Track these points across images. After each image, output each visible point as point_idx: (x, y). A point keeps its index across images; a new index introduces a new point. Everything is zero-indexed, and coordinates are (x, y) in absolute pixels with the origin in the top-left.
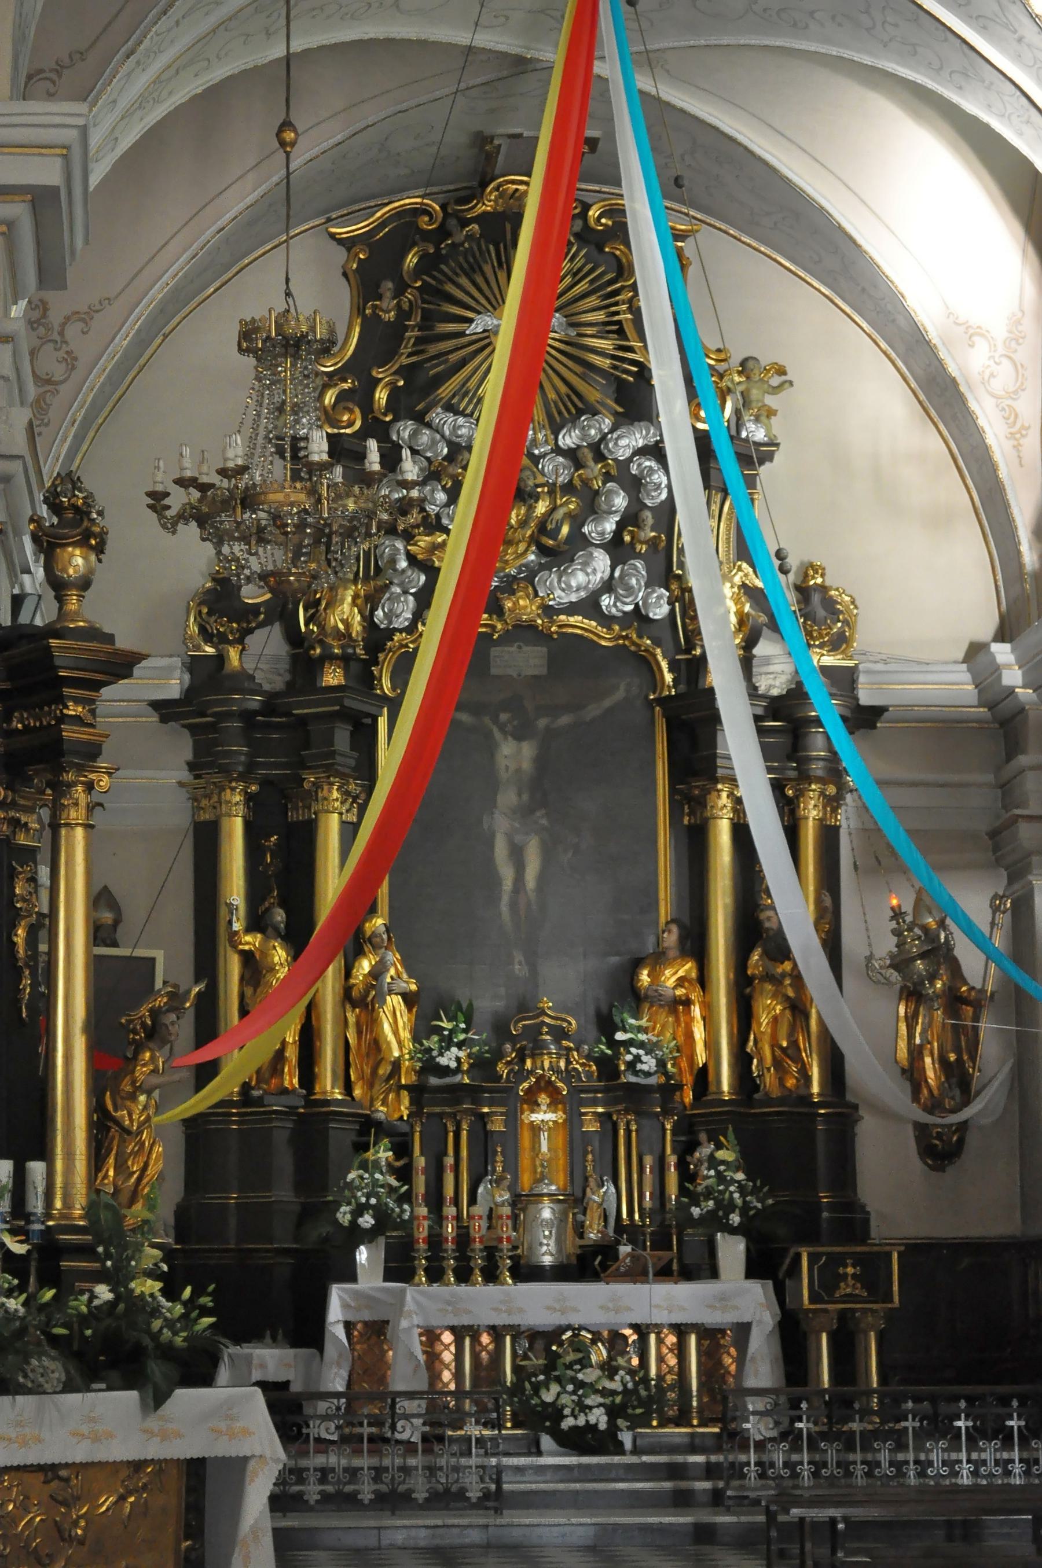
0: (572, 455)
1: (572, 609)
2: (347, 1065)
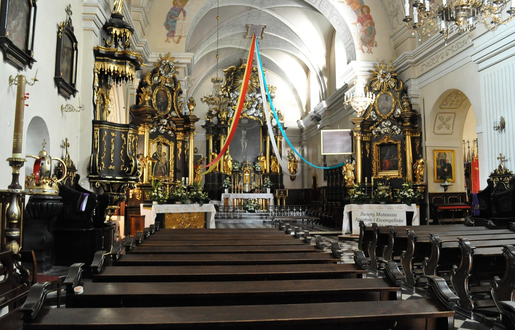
0: (251, 97)
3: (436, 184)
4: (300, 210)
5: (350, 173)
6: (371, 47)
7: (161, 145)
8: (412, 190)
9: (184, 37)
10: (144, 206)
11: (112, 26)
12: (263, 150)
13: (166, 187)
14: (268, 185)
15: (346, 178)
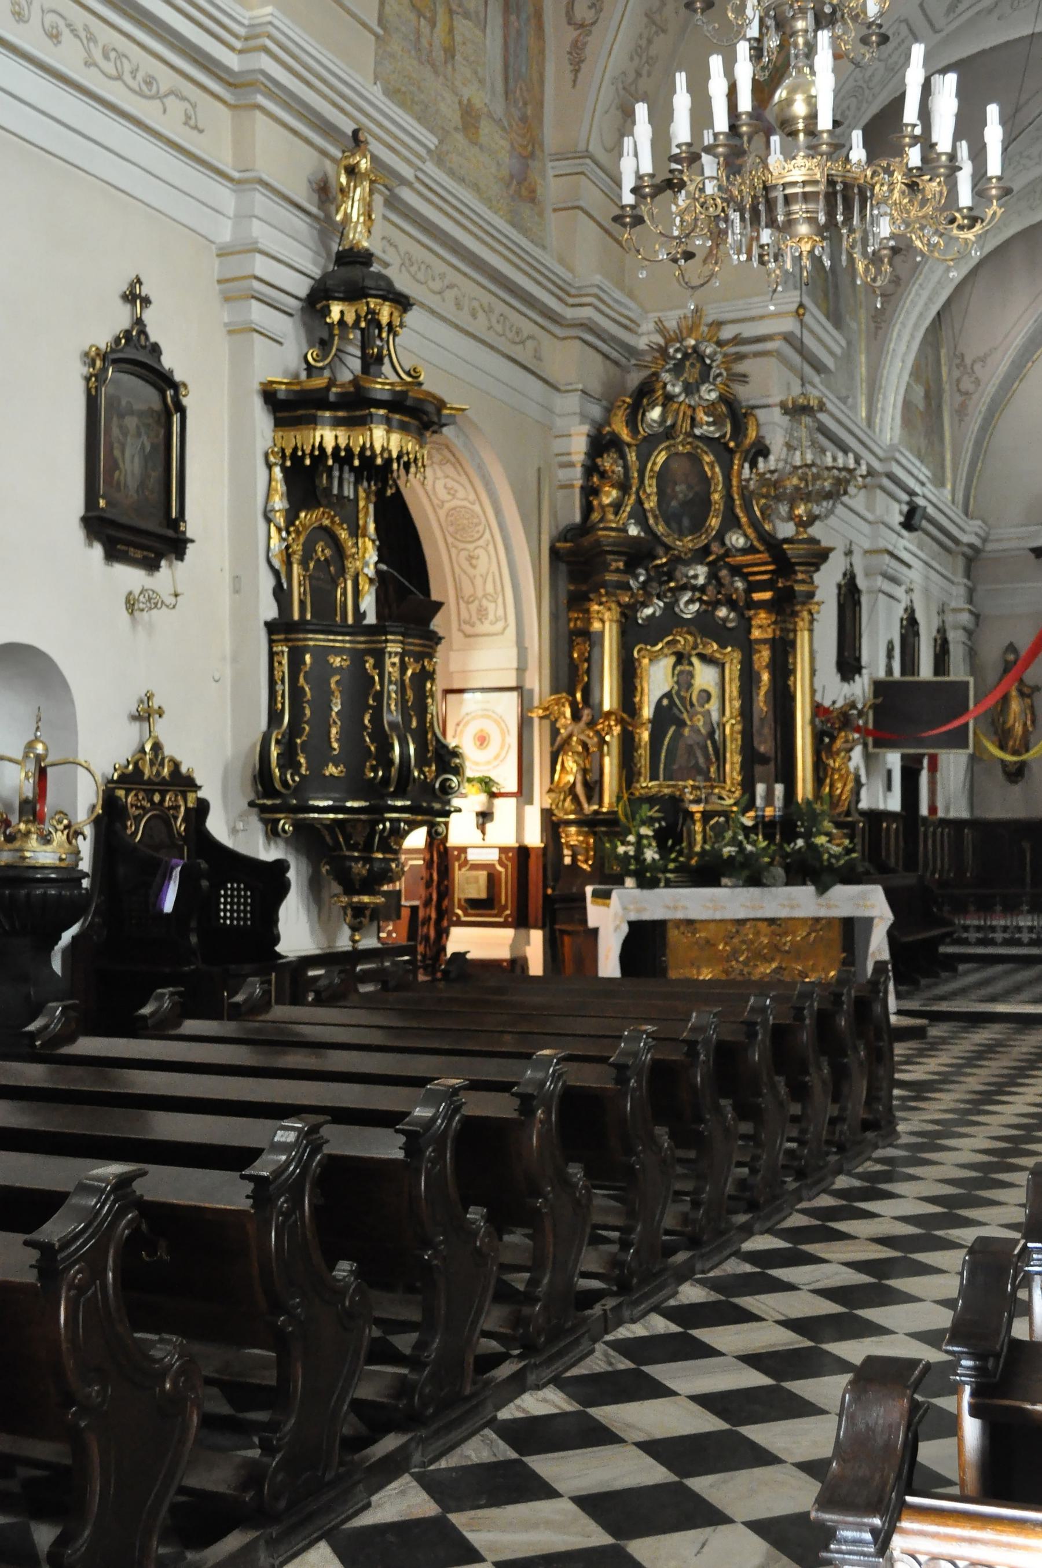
7: (691, 664)
10: (596, 894)
11: (328, 300)
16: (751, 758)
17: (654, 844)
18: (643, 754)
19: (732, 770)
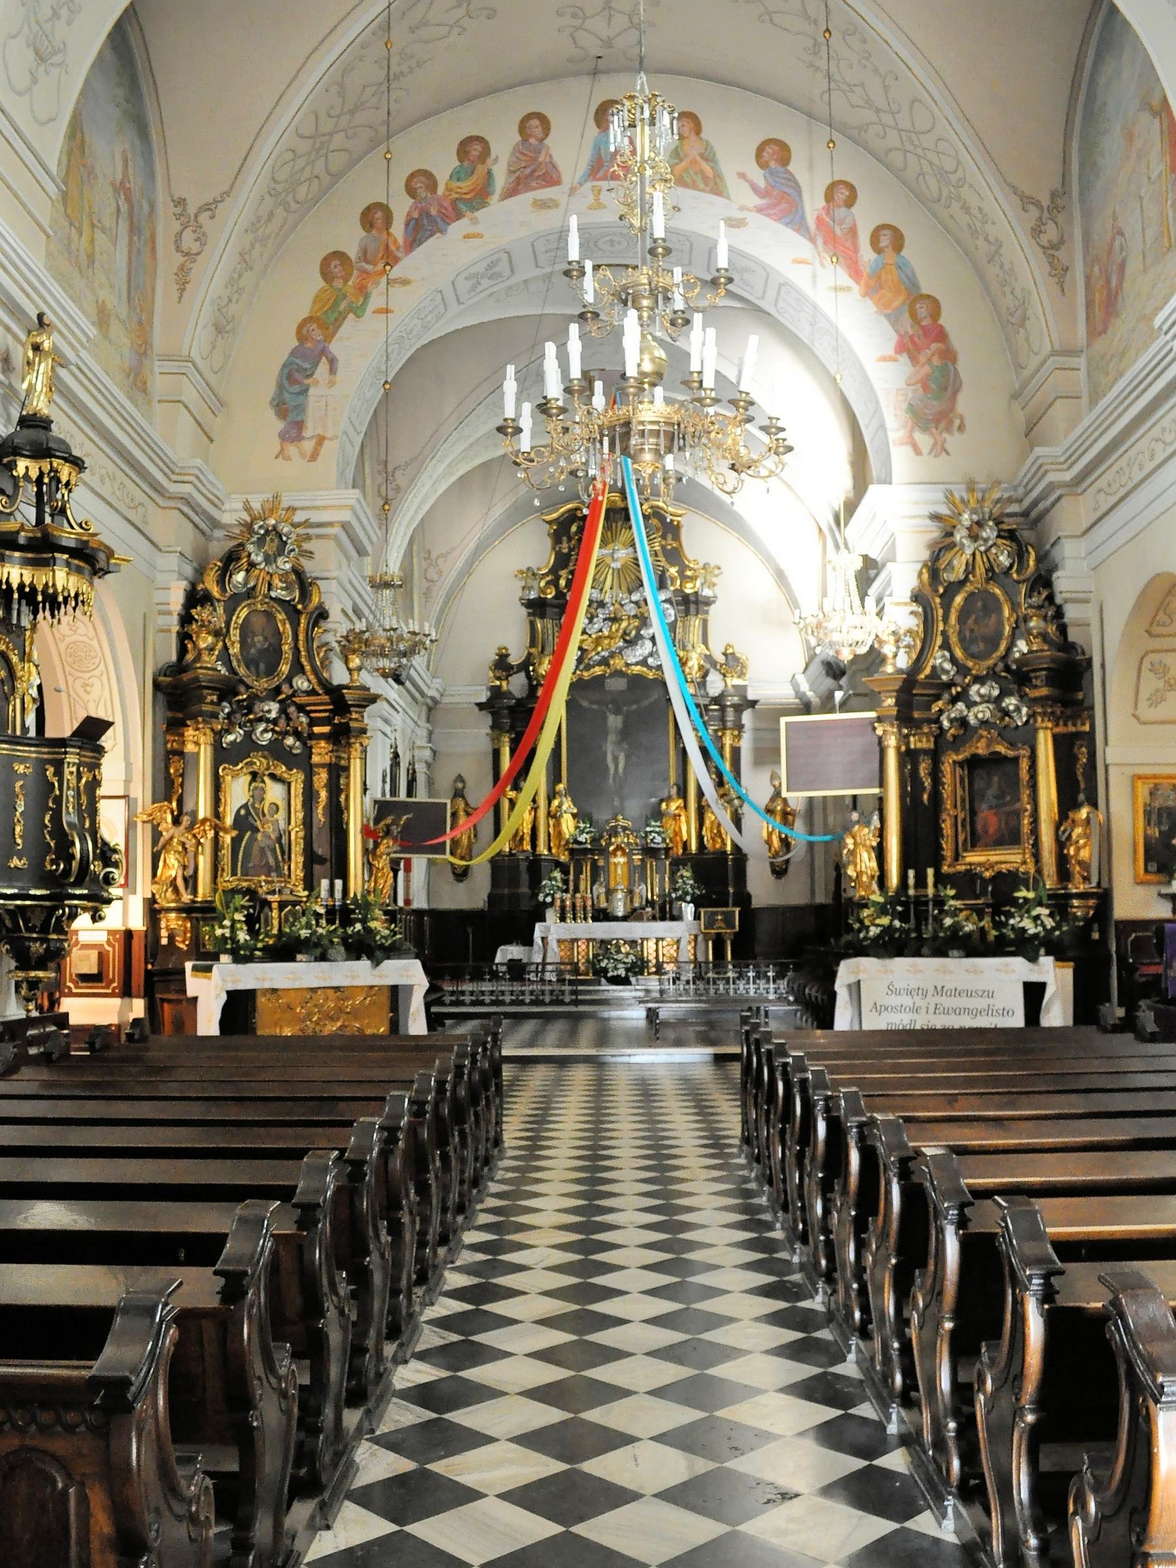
0: (636, 603)
1: (637, 664)
2: (549, 841)
3: (1141, 891)
4: (771, 974)
5: (865, 856)
6: (945, 435)
7: (263, 782)
8: (1047, 912)
9: (331, 439)
10: (195, 969)
12: (677, 779)
13: (271, 910)
14: (686, 893)
15: (851, 872)
16: (311, 858)
17: (245, 928)
18: (226, 853)
19: (297, 867)
